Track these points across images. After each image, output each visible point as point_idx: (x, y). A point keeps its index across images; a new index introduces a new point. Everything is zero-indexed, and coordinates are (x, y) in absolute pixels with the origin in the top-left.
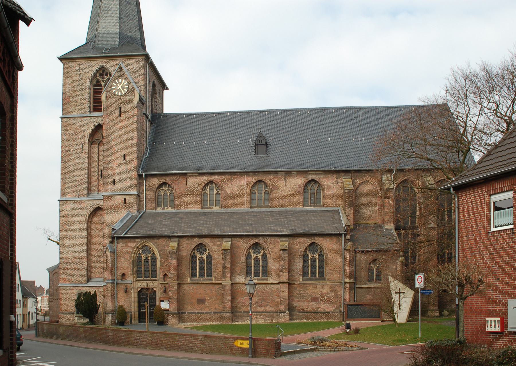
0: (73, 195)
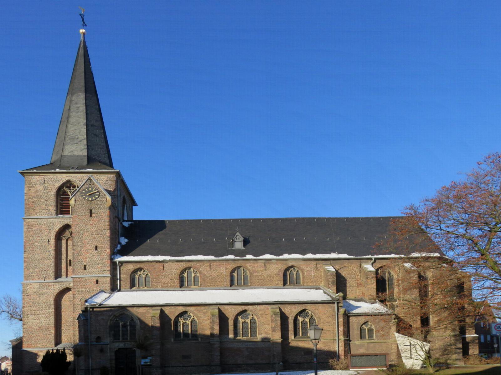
0: (39, 279)
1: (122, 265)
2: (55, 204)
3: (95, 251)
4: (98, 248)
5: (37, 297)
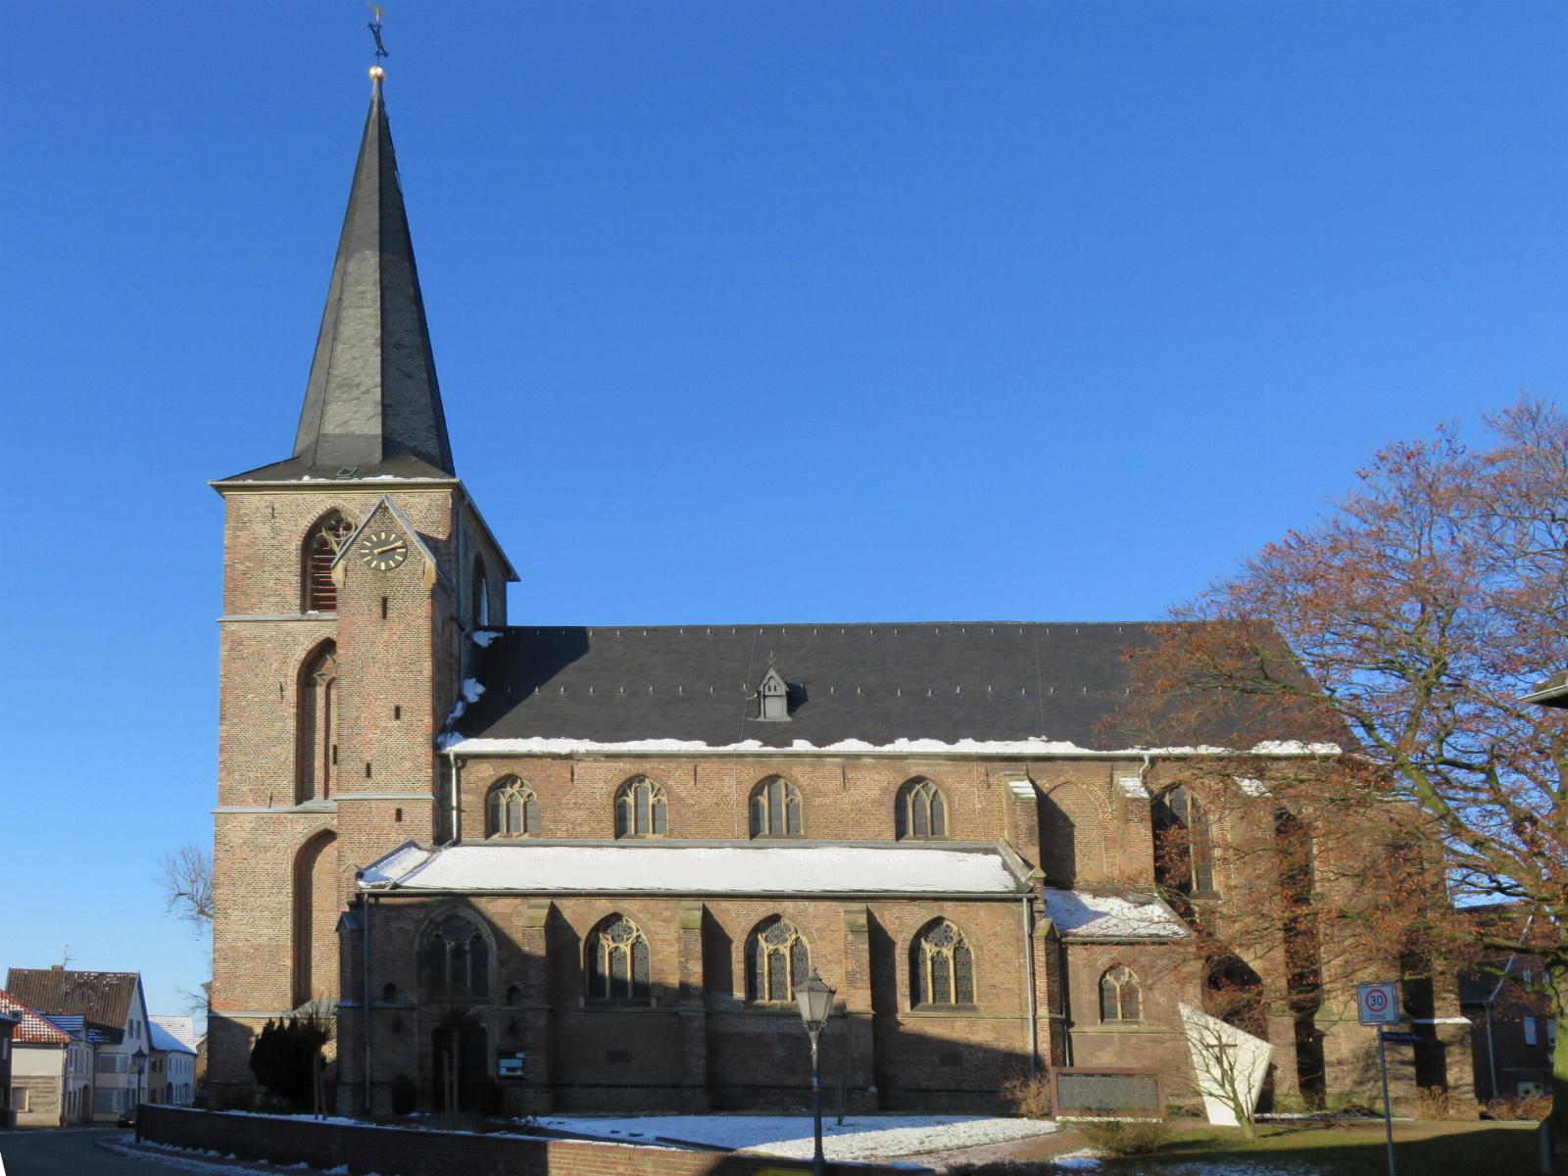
0: (255, 802)
1: (463, 766)
2: (298, 579)
3: (394, 722)
4: (402, 713)
5: (251, 854)
